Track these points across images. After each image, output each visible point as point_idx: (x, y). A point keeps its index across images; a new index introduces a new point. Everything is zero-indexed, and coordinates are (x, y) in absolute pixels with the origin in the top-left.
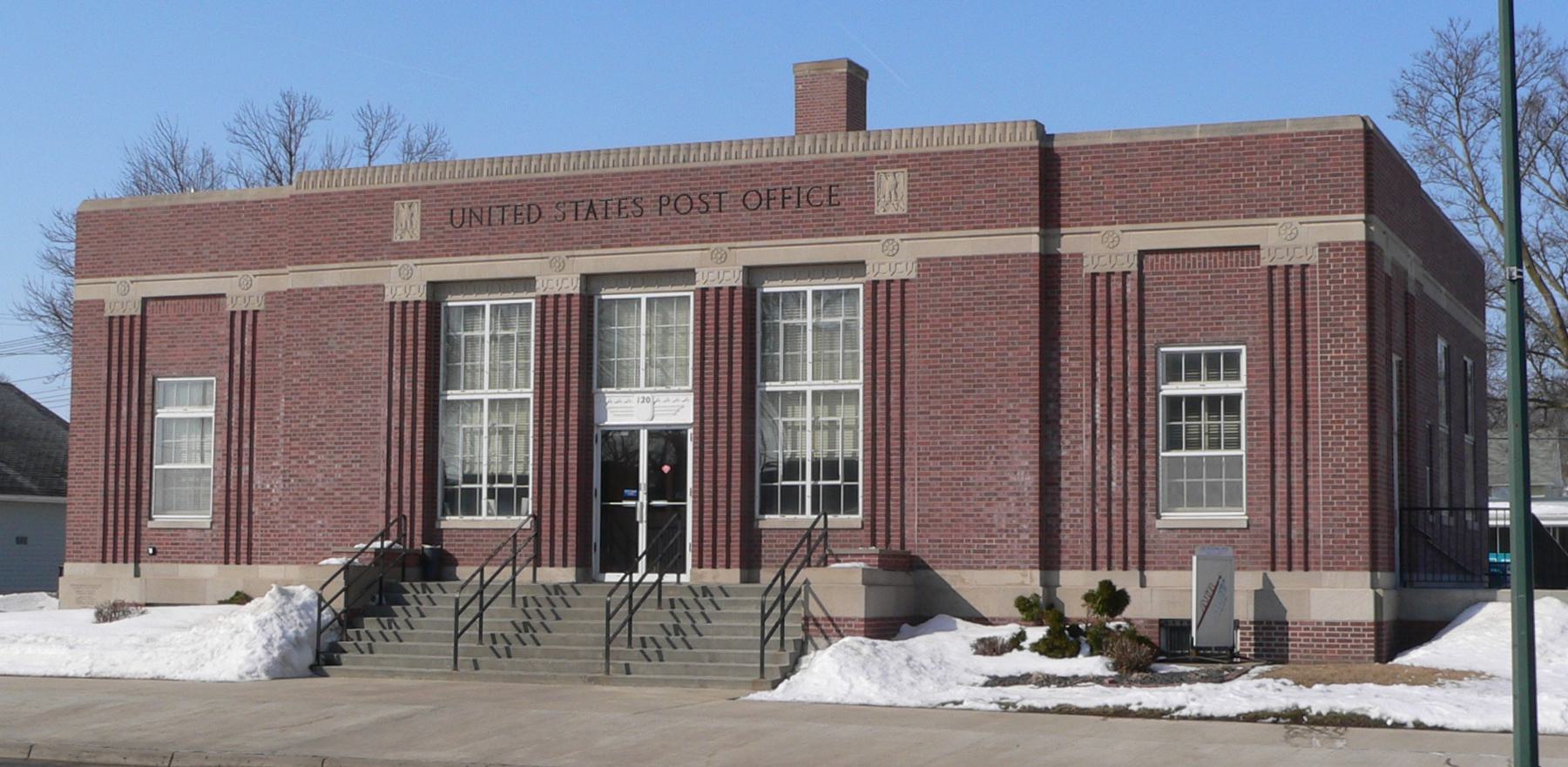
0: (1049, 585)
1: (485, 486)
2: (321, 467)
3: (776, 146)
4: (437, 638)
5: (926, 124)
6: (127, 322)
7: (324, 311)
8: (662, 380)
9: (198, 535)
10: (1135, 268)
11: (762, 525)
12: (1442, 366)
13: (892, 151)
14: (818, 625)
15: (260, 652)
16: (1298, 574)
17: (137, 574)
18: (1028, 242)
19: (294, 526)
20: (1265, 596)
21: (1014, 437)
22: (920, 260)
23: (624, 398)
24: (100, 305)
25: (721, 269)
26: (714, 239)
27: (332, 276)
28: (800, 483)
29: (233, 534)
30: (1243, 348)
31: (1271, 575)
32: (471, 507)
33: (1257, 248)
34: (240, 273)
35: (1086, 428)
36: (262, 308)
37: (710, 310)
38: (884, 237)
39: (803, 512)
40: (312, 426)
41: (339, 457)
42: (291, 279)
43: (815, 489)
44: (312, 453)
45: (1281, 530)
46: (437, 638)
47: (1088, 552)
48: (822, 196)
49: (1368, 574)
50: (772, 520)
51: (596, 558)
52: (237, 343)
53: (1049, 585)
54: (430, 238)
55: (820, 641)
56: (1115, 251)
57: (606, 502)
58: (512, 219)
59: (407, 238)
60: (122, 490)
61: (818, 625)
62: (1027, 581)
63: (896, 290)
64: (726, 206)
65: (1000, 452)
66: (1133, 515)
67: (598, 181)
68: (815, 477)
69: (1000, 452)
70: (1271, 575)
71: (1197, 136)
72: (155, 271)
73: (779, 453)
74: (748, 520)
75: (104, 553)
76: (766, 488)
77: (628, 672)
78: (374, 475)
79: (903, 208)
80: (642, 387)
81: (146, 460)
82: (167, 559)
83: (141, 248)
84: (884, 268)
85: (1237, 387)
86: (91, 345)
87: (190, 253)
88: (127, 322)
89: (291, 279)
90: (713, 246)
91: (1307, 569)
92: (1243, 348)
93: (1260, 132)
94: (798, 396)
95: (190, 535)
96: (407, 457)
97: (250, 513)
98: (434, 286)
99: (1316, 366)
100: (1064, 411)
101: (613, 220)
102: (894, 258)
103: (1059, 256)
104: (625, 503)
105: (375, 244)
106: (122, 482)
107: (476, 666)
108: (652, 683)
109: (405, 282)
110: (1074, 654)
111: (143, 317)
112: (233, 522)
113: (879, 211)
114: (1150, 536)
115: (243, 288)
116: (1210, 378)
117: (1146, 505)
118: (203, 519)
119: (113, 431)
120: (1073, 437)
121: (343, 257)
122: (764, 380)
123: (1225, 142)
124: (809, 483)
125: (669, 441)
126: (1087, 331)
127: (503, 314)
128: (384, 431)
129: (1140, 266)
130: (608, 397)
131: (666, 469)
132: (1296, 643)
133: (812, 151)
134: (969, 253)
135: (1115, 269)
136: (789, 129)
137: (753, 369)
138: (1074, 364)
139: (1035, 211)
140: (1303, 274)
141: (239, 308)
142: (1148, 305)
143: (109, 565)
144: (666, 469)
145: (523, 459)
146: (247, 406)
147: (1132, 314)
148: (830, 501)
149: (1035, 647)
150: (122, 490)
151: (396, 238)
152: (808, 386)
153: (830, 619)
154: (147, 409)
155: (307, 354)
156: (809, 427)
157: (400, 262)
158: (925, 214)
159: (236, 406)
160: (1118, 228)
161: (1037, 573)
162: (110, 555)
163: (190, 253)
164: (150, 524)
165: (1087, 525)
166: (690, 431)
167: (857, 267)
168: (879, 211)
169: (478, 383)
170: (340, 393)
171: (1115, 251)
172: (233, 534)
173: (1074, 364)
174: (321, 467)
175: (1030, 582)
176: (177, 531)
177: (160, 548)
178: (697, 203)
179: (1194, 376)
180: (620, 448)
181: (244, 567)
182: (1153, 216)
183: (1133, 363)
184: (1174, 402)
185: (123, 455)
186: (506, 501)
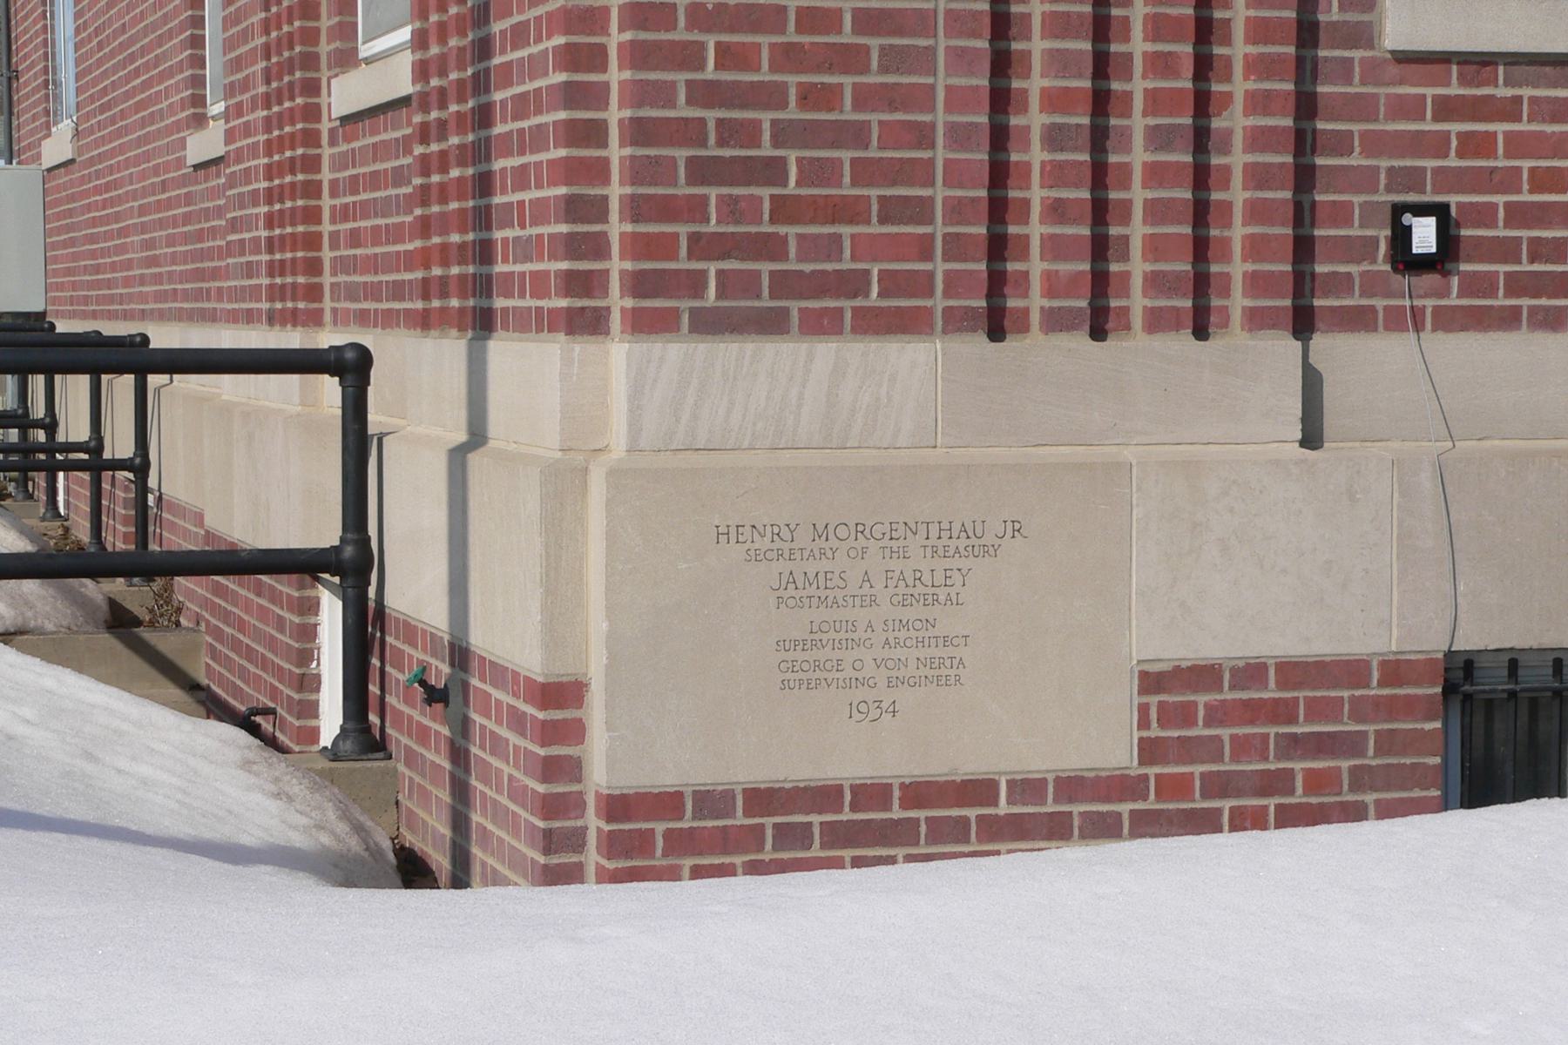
49: (480, 640)
143: (1049, 357)
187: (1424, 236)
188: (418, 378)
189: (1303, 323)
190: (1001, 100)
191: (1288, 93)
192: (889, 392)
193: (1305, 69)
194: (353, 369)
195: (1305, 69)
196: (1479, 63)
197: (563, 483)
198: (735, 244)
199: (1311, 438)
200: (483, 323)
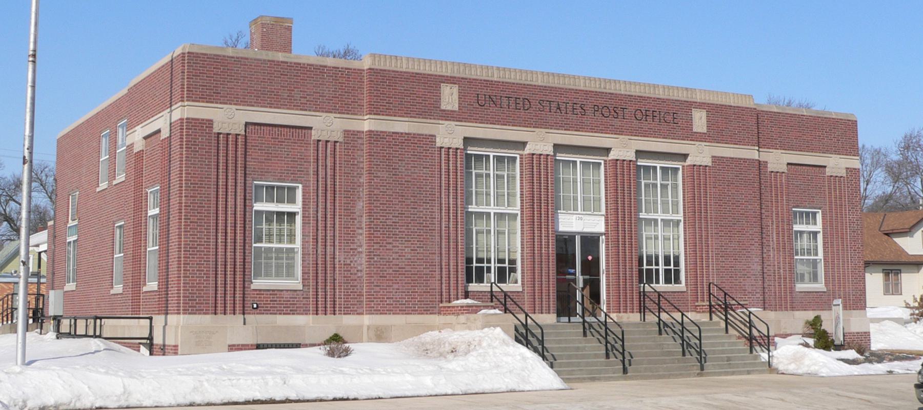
1: (661, 267)
2: (396, 250)
8: (589, 207)
9: (291, 294)
12: (361, 205)
19: (378, 289)
22: (345, 131)
23: (568, 217)
24: (210, 122)
33: (825, 167)
34: (324, 115)
39: (658, 282)
40: (389, 222)
42: (367, 124)
48: (669, 118)
49: (167, 343)
72: (257, 104)
73: (647, 249)
79: (705, 130)
80: (579, 211)
82: (267, 312)
89: (367, 124)
92: (300, 186)
95: (285, 295)
102: (701, 154)
104: (568, 277)
109: (449, 135)
118: (295, 283)
121: (407, 114)
125: (590, 241)
130: (560, 216)
131: (590, 258)
141: (324, 138)
143: (220, 317)
144: (590, 258)
157: (447, 123)
158: (714, 135)
174: (396, 250)
178: (613, 113)
180: (565, 242)
182: (800, 149)
187: (255, 306)
188: (159, 320)
189: (244, 314)
190: (216, 294)
191: (258, 275)
192: (206, 320)
193: (244, 291)
194: (151, 319)
195: (244, 291)
196: (260, 290)
197: (177, 327)
198: (192, 307)
199: (245, 324)
200: (167, 314)
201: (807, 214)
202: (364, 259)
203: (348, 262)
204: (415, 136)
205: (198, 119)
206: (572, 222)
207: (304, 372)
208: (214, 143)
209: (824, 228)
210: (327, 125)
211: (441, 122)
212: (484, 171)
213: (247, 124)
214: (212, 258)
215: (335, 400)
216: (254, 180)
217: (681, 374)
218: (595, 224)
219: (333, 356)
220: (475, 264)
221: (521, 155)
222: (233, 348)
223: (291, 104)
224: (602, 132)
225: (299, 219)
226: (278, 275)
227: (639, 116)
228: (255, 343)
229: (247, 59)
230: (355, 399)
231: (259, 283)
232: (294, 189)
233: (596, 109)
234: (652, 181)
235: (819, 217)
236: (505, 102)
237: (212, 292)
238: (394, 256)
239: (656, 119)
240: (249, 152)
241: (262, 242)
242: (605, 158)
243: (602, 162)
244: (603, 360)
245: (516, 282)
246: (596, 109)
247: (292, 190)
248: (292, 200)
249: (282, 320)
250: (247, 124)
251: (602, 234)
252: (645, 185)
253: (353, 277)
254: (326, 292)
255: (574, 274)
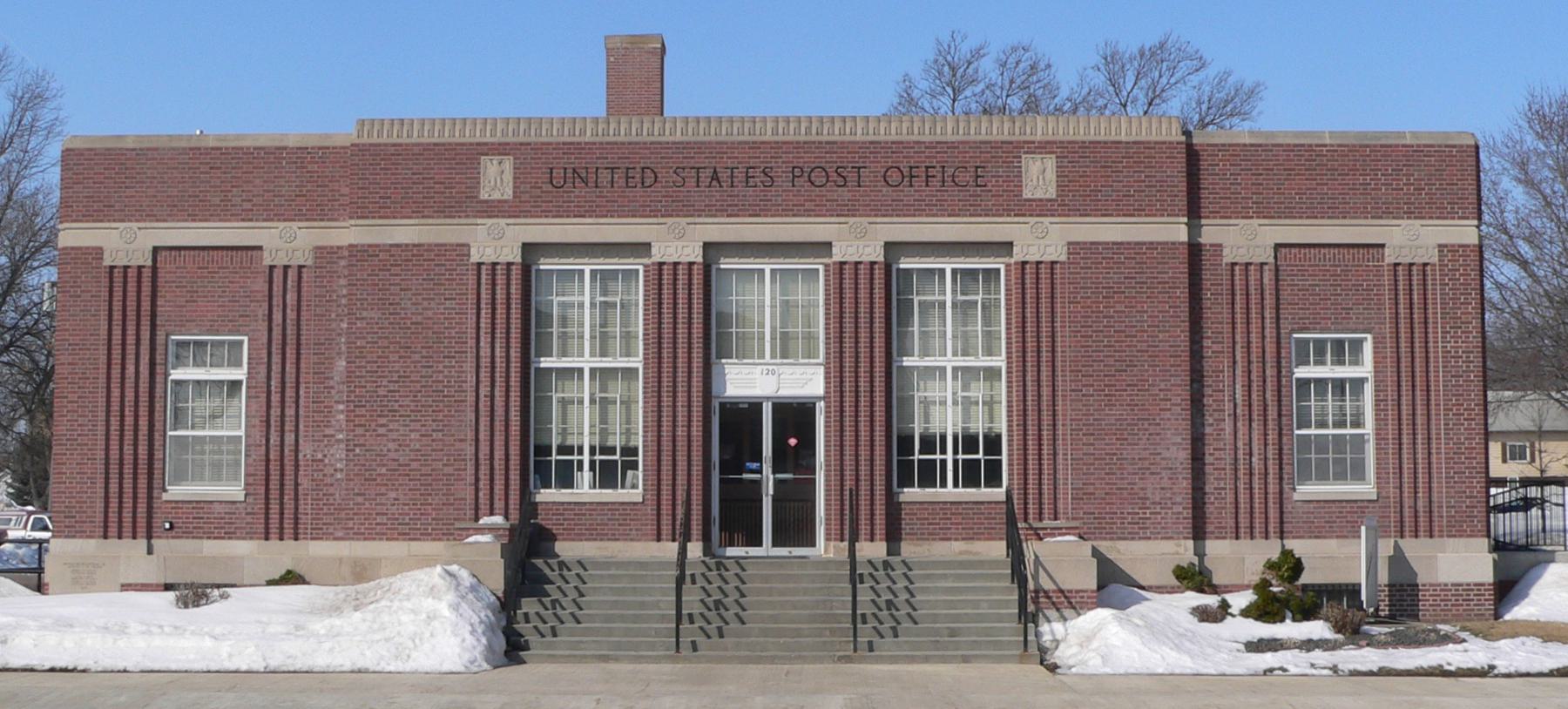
0: (1200, 553)
1: (586, 457)
2: (394, 435)
3: (803, 126)
4: (1000, 618)
5: (569, 114)
6: (132, 274)
7: (395, 270)
9: (227, 508)
10: (149, 263)
11: (902, 498)
13: (1039, 137)
14: (1049, 598)
15: (470, 640)
16: (1424, 541)
17: (150, 551)
18: (1181, 233)
19: (360, 499)
20: (1398, 561)
21: (1167, 415)
22: (1069, 244)
23: (745, 369)
24: (98, 252)
25: (861, 243)
26: (853, 213)
27: (405, 232)
28: (938, 457)
29: (274, 508)
30: (246, 339)
31: (1401, 542)
32: (567, 481)
33: (1383, 246)
34: (282, 225)
35: (1228, 406)
36: (310, 262)
37: (848, 283)
38: (1033, 220)
39: (944, 484)
40: (381, 392)
41: (417, 426)
42: (348, 233)
43: (956, 462)
44: (383, 421)
45: (1407, 502)
46: (1000, 618)
47: (1231, 523)
48: (965, 177)
50: (912, 493)
51: (715, 530)
52: (277, 300)
53: (1200, 553)
54: (525, 197)
55: (1052, 613)
56: (132, 246)
57: (739, 475)
58: (622, 182)
59: (496, 196)
60: (128, 459)
61: (1049, 598)
62: (1181, 550)
63: (292, 274)
64: (865, 181)
65: (1152, 429)
66: (1273, 488)
67: (720, 148)
68: (956, 452)
69: (1152, 429)
70: (1401, 542)
71: (1328, 141)
72: (171, 217)
74: (890, 495)
75: (106, 527)
76: (908, 458)
77: (871, 650)
78: (458, 445)
81: (158, 426)
83: (151, 192)
84: (489, 251)
85: (240, 374)
86: (87, 296)
87: (217, 200)
88: (132, 274)
89: (348, 233)
90: (852, 220)
91: (296, 539)
92: (1369, 336)
93: (1383, 142)
94: (575, 373)
95: (218, 508)
96: (499, 426)
97: (297, 484)
98: (527, 248)
99: (1437, 354)
100: (1208, 391)
101: (740, 188)
102: (1043, 241)
103: (1200, 245)
104: (745, 476)
105: (464, 201)
106: (128, 450)
107: (695, 649)
108: (894, 660)
109: (495, 242)
110: (1282, 620)
111: (154, 268)
112: (274, 494)
113: (1027, 194)
114: (1288, 507)
115: (286, 241)
116: (1317, 363)
117: (153, 484)
118: (234, 490)
119: (116, 393)
120: (1216, 415)
122: (538, 355)
123: (1353, 149)
124: (949, 457)
126: (1226, 316)
127: (604, 279)
128: (471, 398)
129: (155, 260)
132: (1426, 603)
133: (978, 133)
134: (424, 240)
135: (1027, 258)
136: (601, 112)
137: (893, 344)
138: (1216, 347)
139: (1182, 201)
140: (300, 273)
141: (281, 261)
142: (1284, 295)
143: (113, 542)
145: (633, 426)
146: (290, 368)
147: (1269, 301)
148: (607, 475)
149: (1245, 613)
150: (128, 459)
151: (484, 196)
152: (587, 362)
153: (1062, 591)
154: (159, 369)
155: (375, 314)
156: (950, 402)
157: (490, 221)
159: (276, 368)
160: (1256, 222)
161: (1191, 543)
162: (274, 529)
163: (217, 200)
164: (165, 497)
165: (1230, 498)
166: (821, 405)
167: (1006, 247)
168: (1027, 194)
169: (611, 350)
170: (417, 357)
171: (132, 246)
172: (274, 508)
173: (1216, 347)
174: (394, 435)
175: (1184, 552)
176: (199, 504)
177: (178, 523)
178: (834, 177)
179: (1320, 362)
180: (739, 421)
181: (289, 543)
183: (1270, 349)
184: (1304, 384)
185: (129, 420)
186: (607, 475)
201: (1339, 344)
202: (339, 452)
203: (320, 456)
204: (430, 247)
205: (80, 248)
206: (747, 380)
207: (254, 627)
208: (105, 282)
209: (1376, 371)
210: (286, 241)
211: (479, 221)
212: (575, 299)
213: (1278, 246)
214: (101, 455)
215: (52, 670)
216: (1293, 331)
217: (800, 657)
218: (806, 380)
219: (186, 606)
220: (554, 457)
221: (826, 265)
222: (126, 587)
223: (224, 212)
224: (808, 213)
225: (1369, 389)
226: (1340, 476)
227: (894, 177)
228: (162, 581)
229: (156, 149)
230: (84, 671)
231: (1308, 490)
232: (1361, 341)
233: (796, 172)
234: (937, 297)
235: (1368, 348)
236: (605, 177)
237: (100, 505)
238: (391, 446)
239: (936, 182)
240: (161, 292)
241: (1309, 427)
242: (1006, 260)
243: (821, 268)
244: (1014, 625)
245: (634, 486)
246: (796, 172)
247: (1357, 346)
248: (1356, 361)
249: (210, 547)
250: (156, 250)
251: (819, 398)
252: (920, 303)
253: (328, 480)
254: (282, 505)
255: (760, 471)
